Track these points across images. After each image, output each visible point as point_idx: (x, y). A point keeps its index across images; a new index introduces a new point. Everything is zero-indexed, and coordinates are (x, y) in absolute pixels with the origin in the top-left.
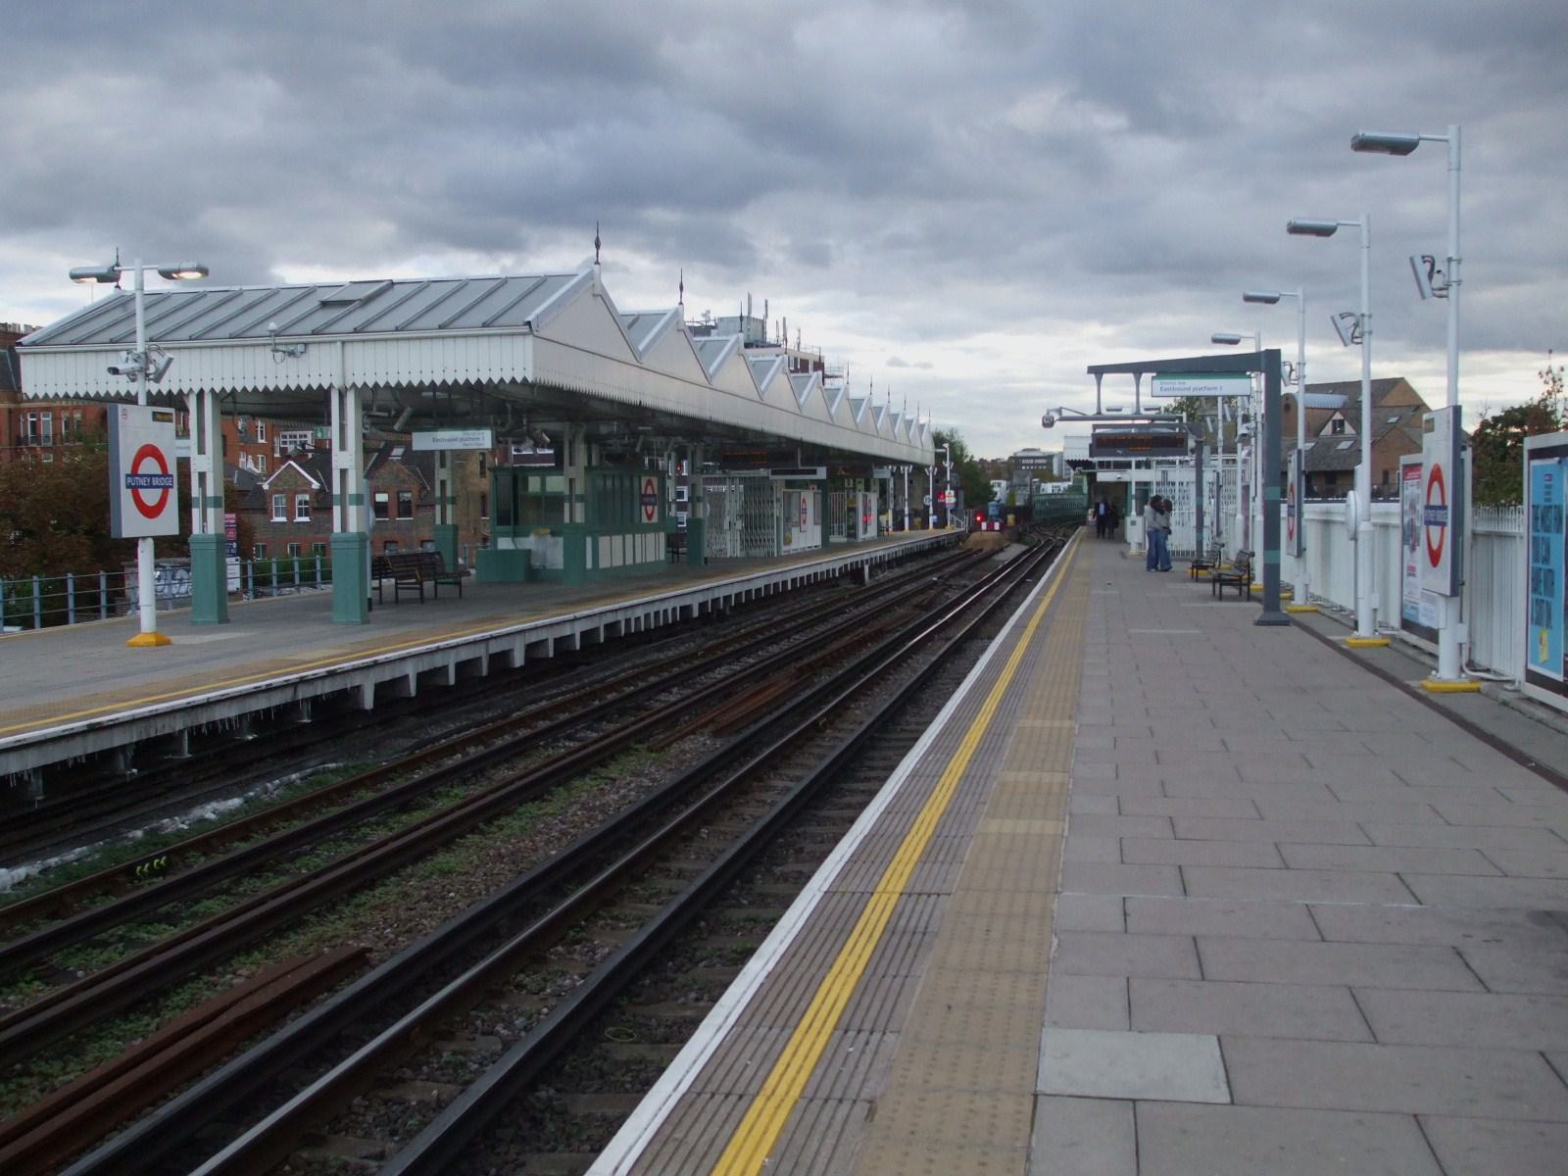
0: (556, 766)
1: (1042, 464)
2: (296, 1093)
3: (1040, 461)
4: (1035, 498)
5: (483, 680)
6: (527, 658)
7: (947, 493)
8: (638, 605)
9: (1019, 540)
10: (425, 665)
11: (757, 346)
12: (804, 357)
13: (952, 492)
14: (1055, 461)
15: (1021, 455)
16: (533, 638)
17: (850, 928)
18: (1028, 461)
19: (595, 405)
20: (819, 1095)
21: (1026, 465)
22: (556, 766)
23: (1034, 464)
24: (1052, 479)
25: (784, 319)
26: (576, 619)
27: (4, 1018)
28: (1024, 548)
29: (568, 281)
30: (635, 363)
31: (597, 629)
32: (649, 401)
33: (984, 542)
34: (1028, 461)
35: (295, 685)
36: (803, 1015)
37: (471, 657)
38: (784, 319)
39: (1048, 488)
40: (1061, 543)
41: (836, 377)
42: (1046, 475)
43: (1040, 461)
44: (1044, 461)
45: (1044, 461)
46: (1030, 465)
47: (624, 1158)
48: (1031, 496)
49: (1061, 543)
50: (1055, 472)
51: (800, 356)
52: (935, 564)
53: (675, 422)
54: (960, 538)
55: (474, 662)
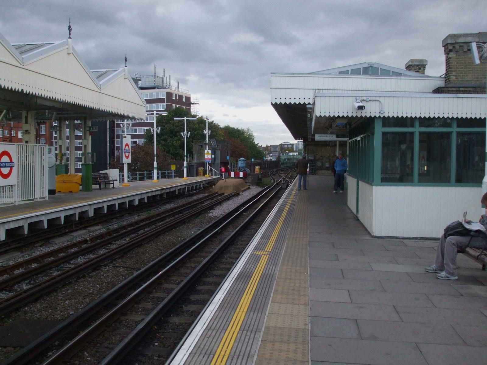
0: (122, 248)
1: (290, 147)
2: (142, 286)
3: (289, 146)
4: (281, 157)
5: (105, 215)
6: (139, 203)
7: (206, 151)
8: (79, 207)
9: (258, 182)
10: (120, 201)
11: (158, 88)
12: (181, 94)
13: (210, 151)
14: (294, 146)
15: (283, 144)
16: (131, 199)
17: (253, 271)
18: (285, 146)
19: (39, 102)
20: (245, 329)
21: (285, 147)
22: (122, 248)
23: (287, 147)
24: (293, 151)
25: (170, 76)
26: (104, 202)
27: (1, 301)
28: (260, 189)
29: (113, 73)
30: (97, 90)
31: (181, 189)
32: (27, 89)
33: (227, 187)
34: (285, 146)
35: (170, 188)
36: (228, 326)
37: (133, 199)
38: (170, 76)
39: (291, 154)
40: (285, 186)
41: (196, 104)
42: (292, 151)
43: (289, 146)
44: (291, 146)
45: (291, 146)
46: (286, 147)
47: (181, 361)
48: (279, 156)
49: (285, 186)
50: (295, 149)
51: (178, 93)
52: (148, 218)
53: (57, 106)
54: (211, 183)
55: (124, 203)
